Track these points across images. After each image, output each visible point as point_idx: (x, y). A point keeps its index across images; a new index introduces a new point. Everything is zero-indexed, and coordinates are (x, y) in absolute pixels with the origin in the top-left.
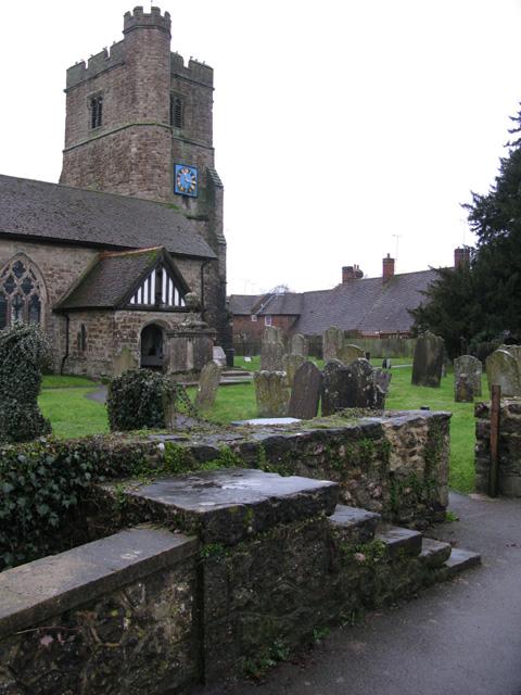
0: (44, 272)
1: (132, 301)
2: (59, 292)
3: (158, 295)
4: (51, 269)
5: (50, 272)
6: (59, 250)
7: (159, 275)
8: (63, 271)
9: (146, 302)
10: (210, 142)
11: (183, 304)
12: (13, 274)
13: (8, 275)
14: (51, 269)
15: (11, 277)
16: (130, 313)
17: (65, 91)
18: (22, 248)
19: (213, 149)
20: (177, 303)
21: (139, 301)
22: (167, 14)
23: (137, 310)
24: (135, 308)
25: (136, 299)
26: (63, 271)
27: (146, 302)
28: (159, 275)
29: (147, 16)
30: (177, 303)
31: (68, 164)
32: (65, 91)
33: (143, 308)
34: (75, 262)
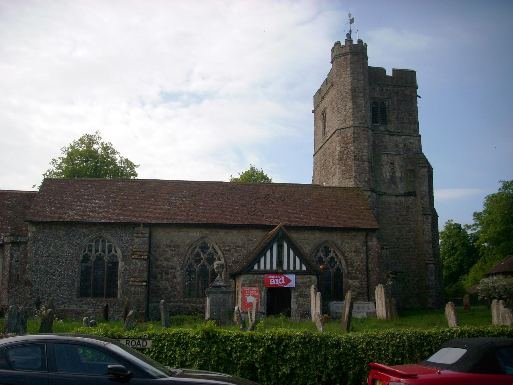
0: (223, 249)
1: (256, 267)
2: (235, 262)
3: (280, 263)
4: (228, 246)
5: (227, 248)
6: (235, 232)
7: (280, 248)
8: (238, 246)
9: (268, 267)
10: (417, 131)
11: (304, 268)
12: (200, 251)
13: (196, 251)
14: (228, 246)
15: (198, 252)
16: (255, 276)
17: (313, 112)
18: (205, 232)
19: (420, 136)
20: (298, 268)
21: (262, 267)
22: (360, 41)
23: (260, 274)
24: (259, 272)
25: (259, 266)
26: (238, 246)
27: (268, 267)
28: (280, 248)
29: (344, 47)
30: (298, 268)
31: (42, 187)
32: (313, 112)
33: (265, 272)
34: (248, 240)
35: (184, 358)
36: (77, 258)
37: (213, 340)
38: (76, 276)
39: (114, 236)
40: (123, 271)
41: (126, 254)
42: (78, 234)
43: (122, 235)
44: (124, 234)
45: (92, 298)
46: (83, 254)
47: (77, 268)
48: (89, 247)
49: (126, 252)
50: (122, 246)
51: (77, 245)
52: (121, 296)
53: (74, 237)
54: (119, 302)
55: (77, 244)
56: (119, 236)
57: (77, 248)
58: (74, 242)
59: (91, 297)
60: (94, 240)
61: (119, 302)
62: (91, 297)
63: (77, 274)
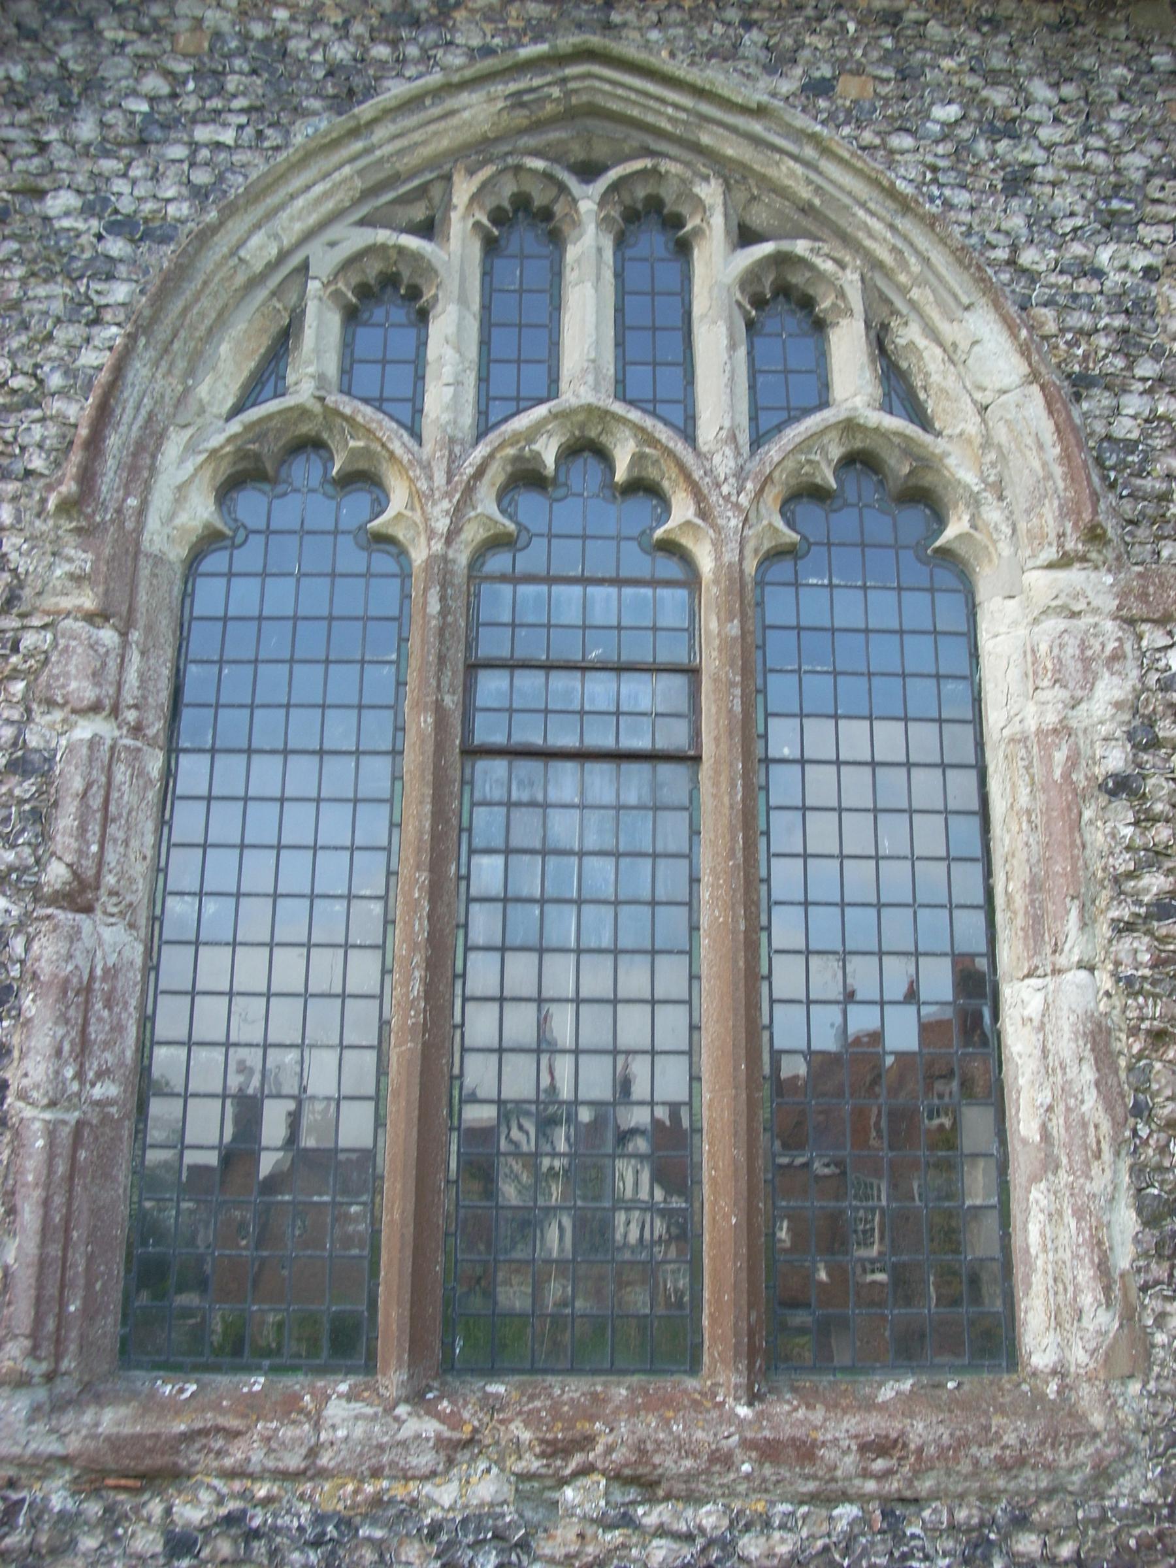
30: (644, 1195)
35: (67, 1538)
36: (87, 477)
37: (378, 1534)
38: (56, 874)
39: (856, 116)
40: (1116, 759)
41: (1126, 428)
42: (143, 64)
43: (999, 97)
44: (1040, 90)
45: (417, 1398)
46: (235, 427)
47: (83, 690)
48: (351, 316)
49: (1116, 386)
50: (1032, 277)
51: (116, 247)
52: (1129, 1316)
53: (68, 109)
54: (1103, 1474)
55: (123, 226)
56: (952, 112)
57: (120, 292)
58: (59, 203)
59: (392, 1380)
60: (463, 189)
61: (1103, 1474)
62: (392, 1380)
63: (65, 821)
